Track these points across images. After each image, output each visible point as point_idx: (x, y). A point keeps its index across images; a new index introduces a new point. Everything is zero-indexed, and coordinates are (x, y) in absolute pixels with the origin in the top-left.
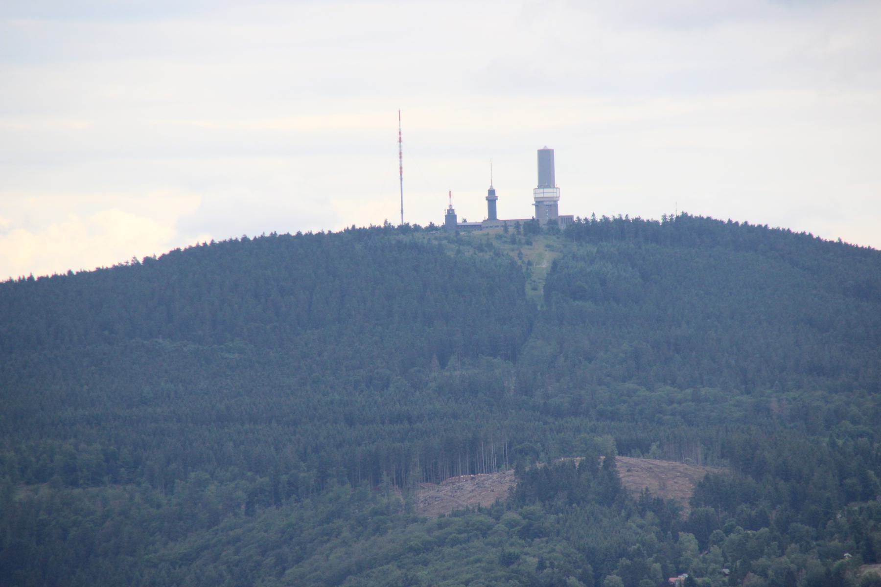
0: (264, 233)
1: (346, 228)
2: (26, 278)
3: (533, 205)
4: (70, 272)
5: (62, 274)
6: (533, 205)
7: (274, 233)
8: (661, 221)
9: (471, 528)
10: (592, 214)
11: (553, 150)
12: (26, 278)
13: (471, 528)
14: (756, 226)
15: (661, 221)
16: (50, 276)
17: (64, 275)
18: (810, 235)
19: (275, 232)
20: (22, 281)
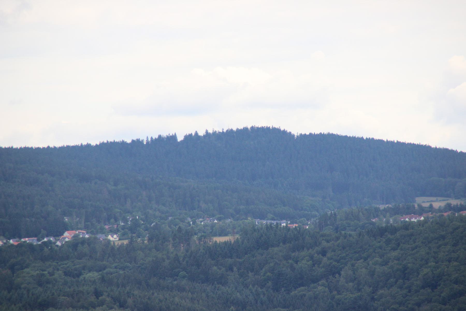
0: (247, 126)
1: (138, 139)
2: (424, 145)
3: (26, 146)
4: (82, 145)
5: (382, 139)
6: (26, 146)
7: (174, 134)
8: (313, 134)
9: (352, 223)
10: (146, 137)
11: (132, 140)
12: (424, 145)
13: (352, 223)
14: (180, 138)
15: (313, 134)
16: (19, 148)
17: (294, 136)
18: (373, 139)
19: (175, 134)
20: (9, 148)
